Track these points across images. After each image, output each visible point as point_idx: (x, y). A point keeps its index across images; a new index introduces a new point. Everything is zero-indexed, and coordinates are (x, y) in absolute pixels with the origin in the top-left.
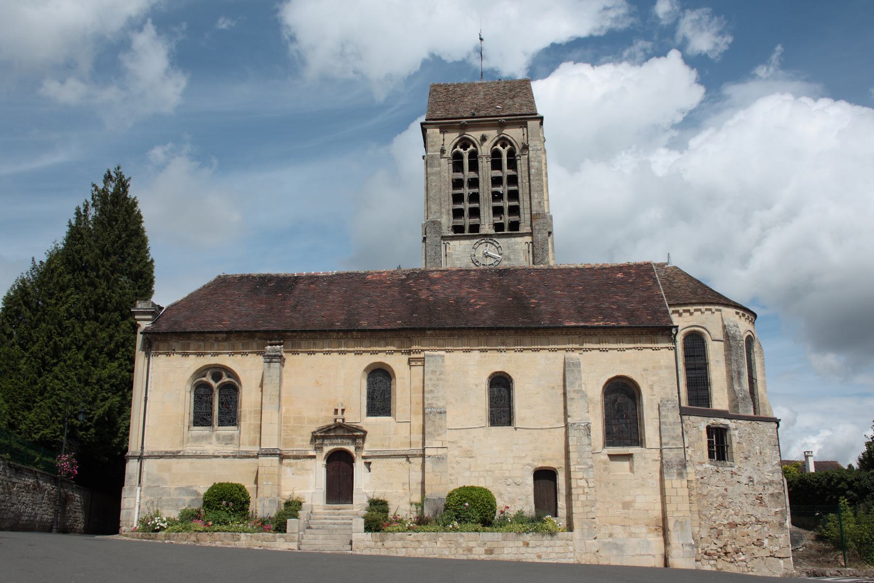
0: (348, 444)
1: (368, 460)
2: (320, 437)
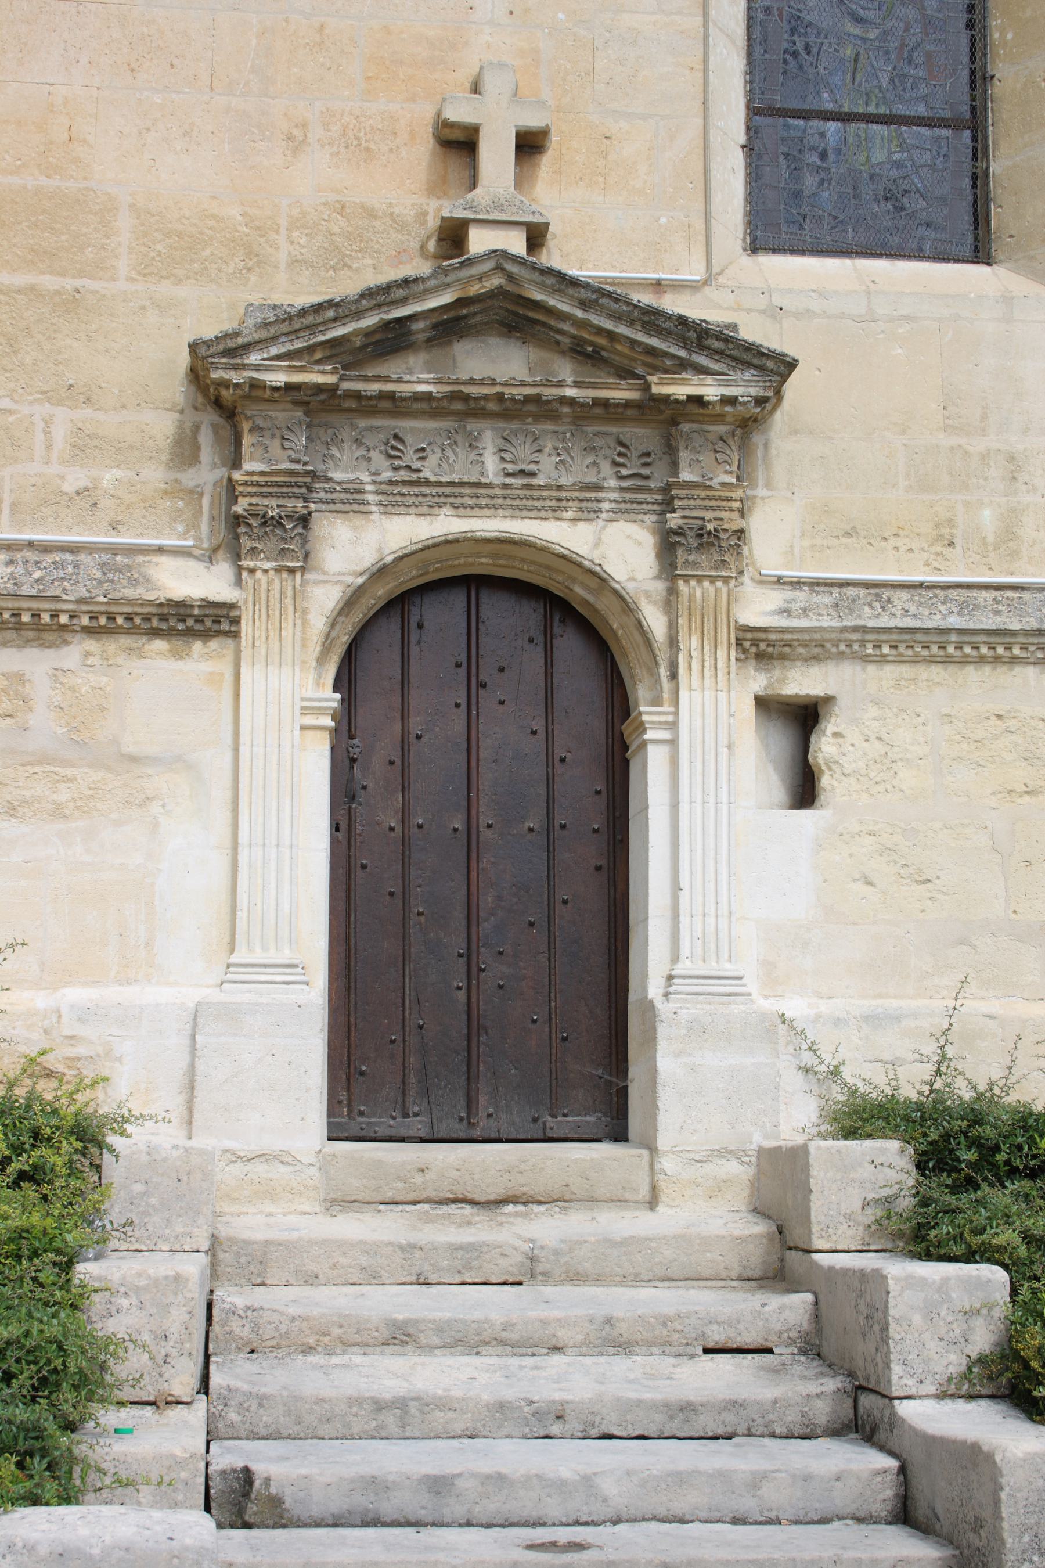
0: (584, 499)
1: (801, 682)
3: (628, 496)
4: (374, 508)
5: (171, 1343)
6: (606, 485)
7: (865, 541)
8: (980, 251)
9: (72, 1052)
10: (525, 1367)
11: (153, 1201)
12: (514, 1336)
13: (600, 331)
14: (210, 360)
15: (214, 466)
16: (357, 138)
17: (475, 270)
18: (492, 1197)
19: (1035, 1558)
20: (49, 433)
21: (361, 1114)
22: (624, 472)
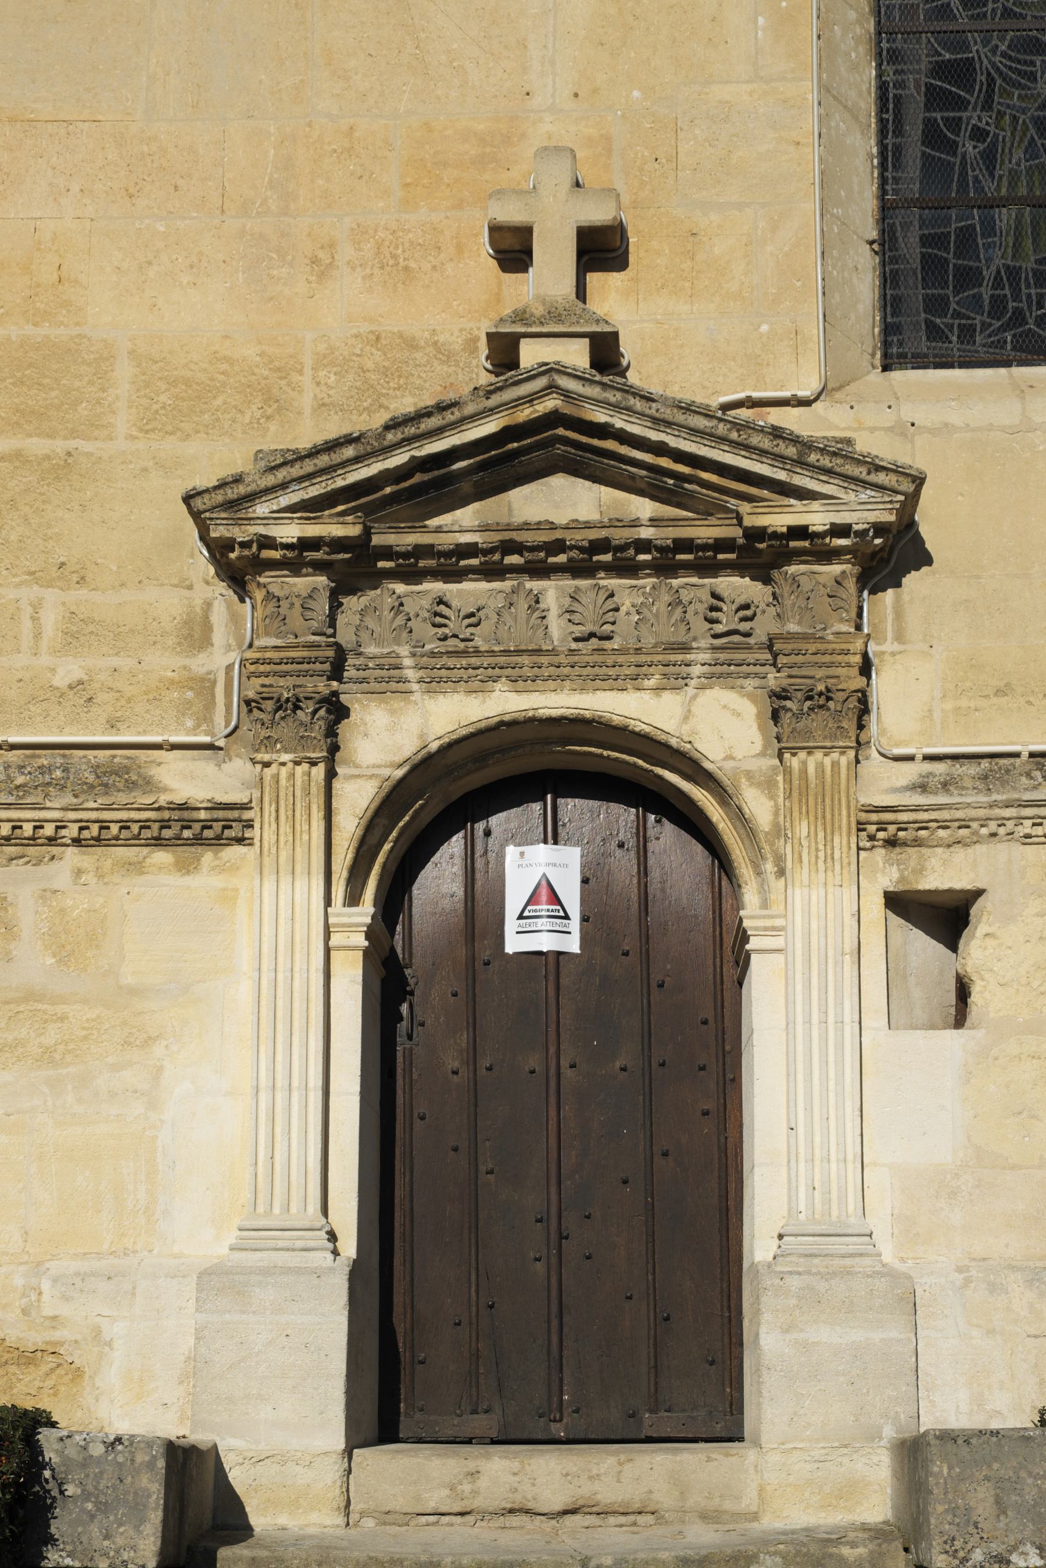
0: (668, 664)
1: (941, 873)
3: (722, 656)
4: (415, 687)
6: (694, 645)
7: (1022, 700)
14: (207, 515)
15: (228, 648)
16: (394, 256)
20: (38, 619)
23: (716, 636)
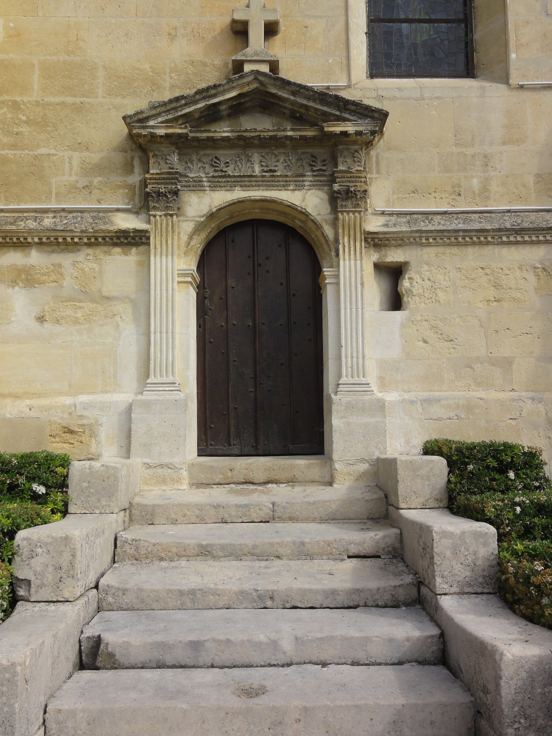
1: (395, 256)
2: (166, 145)
3: (316, 178)
4: (208, 188)
5: (63, 571)
6: (306, 174)
8: (469, 71)
9: (80, 422)
10: (261, 567)
11: (92, 490)
12: (257, 551)
13: (302, 105)
16: (198, 33)
17: (245, 80)
18: (261, 481)
19: (522, 721)
21: (211, 445)
22: (315, 169)
23: (314, 171)
